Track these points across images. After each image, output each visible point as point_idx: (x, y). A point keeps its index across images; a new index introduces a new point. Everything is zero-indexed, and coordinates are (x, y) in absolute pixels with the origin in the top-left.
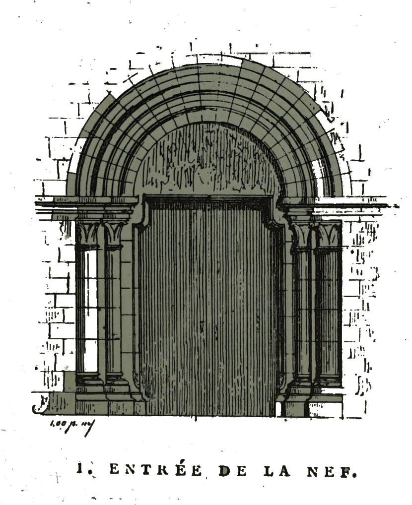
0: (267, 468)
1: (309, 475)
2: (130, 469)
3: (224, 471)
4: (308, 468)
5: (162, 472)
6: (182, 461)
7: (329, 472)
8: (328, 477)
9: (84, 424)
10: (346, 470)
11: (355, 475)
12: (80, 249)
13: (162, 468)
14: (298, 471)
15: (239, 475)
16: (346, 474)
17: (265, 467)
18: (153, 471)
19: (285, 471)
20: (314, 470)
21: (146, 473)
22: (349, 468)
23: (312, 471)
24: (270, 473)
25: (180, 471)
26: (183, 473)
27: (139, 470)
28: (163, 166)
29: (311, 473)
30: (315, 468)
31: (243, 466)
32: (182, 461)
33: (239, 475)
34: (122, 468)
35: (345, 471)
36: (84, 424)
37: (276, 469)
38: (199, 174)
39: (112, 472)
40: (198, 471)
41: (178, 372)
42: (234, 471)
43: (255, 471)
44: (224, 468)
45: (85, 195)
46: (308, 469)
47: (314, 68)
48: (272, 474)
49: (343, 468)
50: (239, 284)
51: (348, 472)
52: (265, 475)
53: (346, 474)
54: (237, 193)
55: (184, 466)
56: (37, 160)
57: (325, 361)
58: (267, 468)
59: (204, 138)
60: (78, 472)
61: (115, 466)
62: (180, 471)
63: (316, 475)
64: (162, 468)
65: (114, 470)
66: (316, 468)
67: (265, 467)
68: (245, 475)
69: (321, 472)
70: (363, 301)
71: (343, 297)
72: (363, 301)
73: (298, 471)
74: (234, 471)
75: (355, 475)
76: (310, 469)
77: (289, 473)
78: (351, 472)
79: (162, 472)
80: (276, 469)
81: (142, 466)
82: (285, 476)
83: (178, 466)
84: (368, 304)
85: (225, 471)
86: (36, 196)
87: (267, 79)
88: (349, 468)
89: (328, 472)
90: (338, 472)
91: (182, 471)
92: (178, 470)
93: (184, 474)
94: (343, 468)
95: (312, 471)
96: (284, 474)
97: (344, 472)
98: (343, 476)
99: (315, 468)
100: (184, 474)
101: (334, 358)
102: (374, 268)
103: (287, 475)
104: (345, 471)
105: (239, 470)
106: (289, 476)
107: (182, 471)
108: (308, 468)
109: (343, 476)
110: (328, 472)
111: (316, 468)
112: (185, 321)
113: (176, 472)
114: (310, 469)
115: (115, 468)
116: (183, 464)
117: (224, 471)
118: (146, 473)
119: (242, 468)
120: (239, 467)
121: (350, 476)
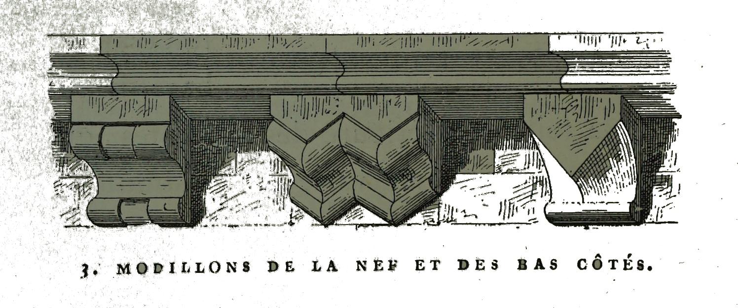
0: (315, 263)
1: (358, 270)
2: (232, 268)
3: (273, 266)
4: (227, 263)
6: (629, 255)
7: (289, 268)
9: (325, 216)
20: (363, 264)
23: (361, 265)
24: (201, 270)
26: (422, 268)
28: (577, 75)
30: (363, 261)
32: (629, 255)
34: (488, 265)
36: (325, 216)
37: (324, 264)
39: (417, 269)
42: (473, 265)
43: (259, 267)
44: (273, 264)
46: (357, 263)
48: (320, 269)
50: (300, 105)
55: (631, 261)
57: (333, 168)
58: (315, 263)
59: (664, 69)
60: (433, 269)
61: (482, 262)
63: (365, 269)
64: (523, 262)
66: (235, 263)
68: (423, 269)
69: (371, 266)
70: (672, 152)
72: (672, 152)
74: (473, 265)
76: (359, 262)
80: (324, 264)
82: (332, 270)
83: (625, 261)
84: (676, 154)
85: (274, 266)
91: (291, 268)
92: (287, 266)
95: (361, 265)
96: (539, 267)
99: (363, 261)
103: (335, 270)
105: (478, 264)
107: (291, 268)
108: (227, 263)
111: (365, 262)
113: (623, 267)
114: (359, 262)
115: (481, 264)
117: (273, 266)
118: (613, 268)
119: (480, 262)
120: (477, 261)
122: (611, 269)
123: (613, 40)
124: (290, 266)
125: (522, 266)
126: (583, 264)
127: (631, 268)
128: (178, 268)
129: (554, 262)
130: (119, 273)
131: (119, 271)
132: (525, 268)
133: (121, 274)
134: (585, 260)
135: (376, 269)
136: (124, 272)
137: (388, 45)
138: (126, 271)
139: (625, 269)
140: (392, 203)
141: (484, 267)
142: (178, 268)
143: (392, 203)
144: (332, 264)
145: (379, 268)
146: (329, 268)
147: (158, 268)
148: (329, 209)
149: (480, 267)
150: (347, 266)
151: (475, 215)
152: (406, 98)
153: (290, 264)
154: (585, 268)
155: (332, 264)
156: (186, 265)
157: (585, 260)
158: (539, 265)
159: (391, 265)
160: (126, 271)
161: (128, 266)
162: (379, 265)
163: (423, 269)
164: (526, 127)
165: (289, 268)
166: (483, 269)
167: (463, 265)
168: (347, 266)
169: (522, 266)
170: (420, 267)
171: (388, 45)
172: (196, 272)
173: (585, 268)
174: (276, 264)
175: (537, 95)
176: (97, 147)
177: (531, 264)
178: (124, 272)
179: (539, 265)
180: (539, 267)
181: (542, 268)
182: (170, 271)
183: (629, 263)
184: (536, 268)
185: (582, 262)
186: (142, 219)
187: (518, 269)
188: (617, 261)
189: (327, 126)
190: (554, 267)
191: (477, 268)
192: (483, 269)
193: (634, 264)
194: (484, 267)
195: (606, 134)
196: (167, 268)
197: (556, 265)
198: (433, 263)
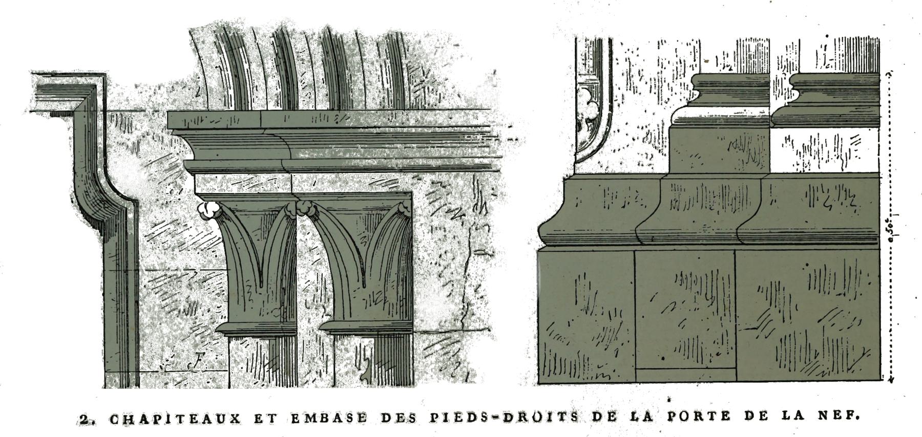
0: (785, 412)
1: (820, 418)
3: (749, 415)
7: (763, 416)
8: (295, 424)
11: (858, 418)
13: (128, 418)
15: (761, 419)
16: (850, 416)
17: (746, 412)
18: (186, 419)
19: (648, 417)
21: (562, 419)
22: (853, 411)
23: (823, 415)
27: (706, 417)
31: (401, 414)
33: (761, 419)
35: (850, 413)
37: (792, 414)
38: (677, 56)
40: (838, 415)
41: (318, 342)
46: (819, 414)
49: (848, 411)
51: (852, 415)
52: (783, 419)
53: (850, 416)
54: (300, 78)
56: (855, 151)
58: (785, 412)
63: (826, 418)
68: (766, 419)
69: (830, 415)
74: (757, 416)
75: (858, 418)
76: (821, 413)
77: (803, 417)
78: (855, 415)
79: (522, 419)
80: (792, 414)
81: (177, 416)
89: (837, 414)
90: (844, 414)
94: (848, 411)
95: (823, 415)
96: (206, 421)
97: (849, 415)
100: (461, 421)
102: (762, 40)
103: (801, 418)
104: (850, 413)
105: (192, 418)
106: (342, 422)
107: (297, 419)
109: (848, 418)
110: (837, 414)
112: (818, 277)
117: (749, 415)
118: (562, 419)
121: (853, 418)
122: (382, 422)
123: (785, 97)
124: (459, 417)
125: (324, 420)
126: (115, 420)
127: (461, 421)
128: (451, 417)
129: (349, 415)
130: (307, 422)
131: (820, 416)
132: (327, 420)
133: (308, 422)
134: (117, 416)
136: (311, 421)
138: (312, 420)
140: (735, 370)
142: (451, 417)
143: (735, 370)
144: (799, 413)
145: (401, 420)
146: (204, 421)
147: (485, 418)
148: (117, 343)
150: (811, 415)
153: (458, 415)
154: (117, 423)
155: (799, 413)
157: (117, 416)
158: (144, 419)
159: (649, 417)
160: (312, 420)
161: (314, 416)
162: (613, 416)
163: (766, 419)
165: (763, 416)
167: (725, 415)
168: (811, 415)
169: (324, 420)
170: (763, 418)
173: (117, 423)
175: (190, 127)
176: (595, 80)
178: (311, 421)
179: (144, 420)
180: (647, 419)
181: (340, 421)
182: (745, 417)
183: (764, 414)
184: (796, 419)
185: (115, 417)
186: (359, 349)
187: (668, 420)
188: (715, 413)
189: (63, 74)
192: (298, 422)
196: (442, 417)
198: (178, 417)
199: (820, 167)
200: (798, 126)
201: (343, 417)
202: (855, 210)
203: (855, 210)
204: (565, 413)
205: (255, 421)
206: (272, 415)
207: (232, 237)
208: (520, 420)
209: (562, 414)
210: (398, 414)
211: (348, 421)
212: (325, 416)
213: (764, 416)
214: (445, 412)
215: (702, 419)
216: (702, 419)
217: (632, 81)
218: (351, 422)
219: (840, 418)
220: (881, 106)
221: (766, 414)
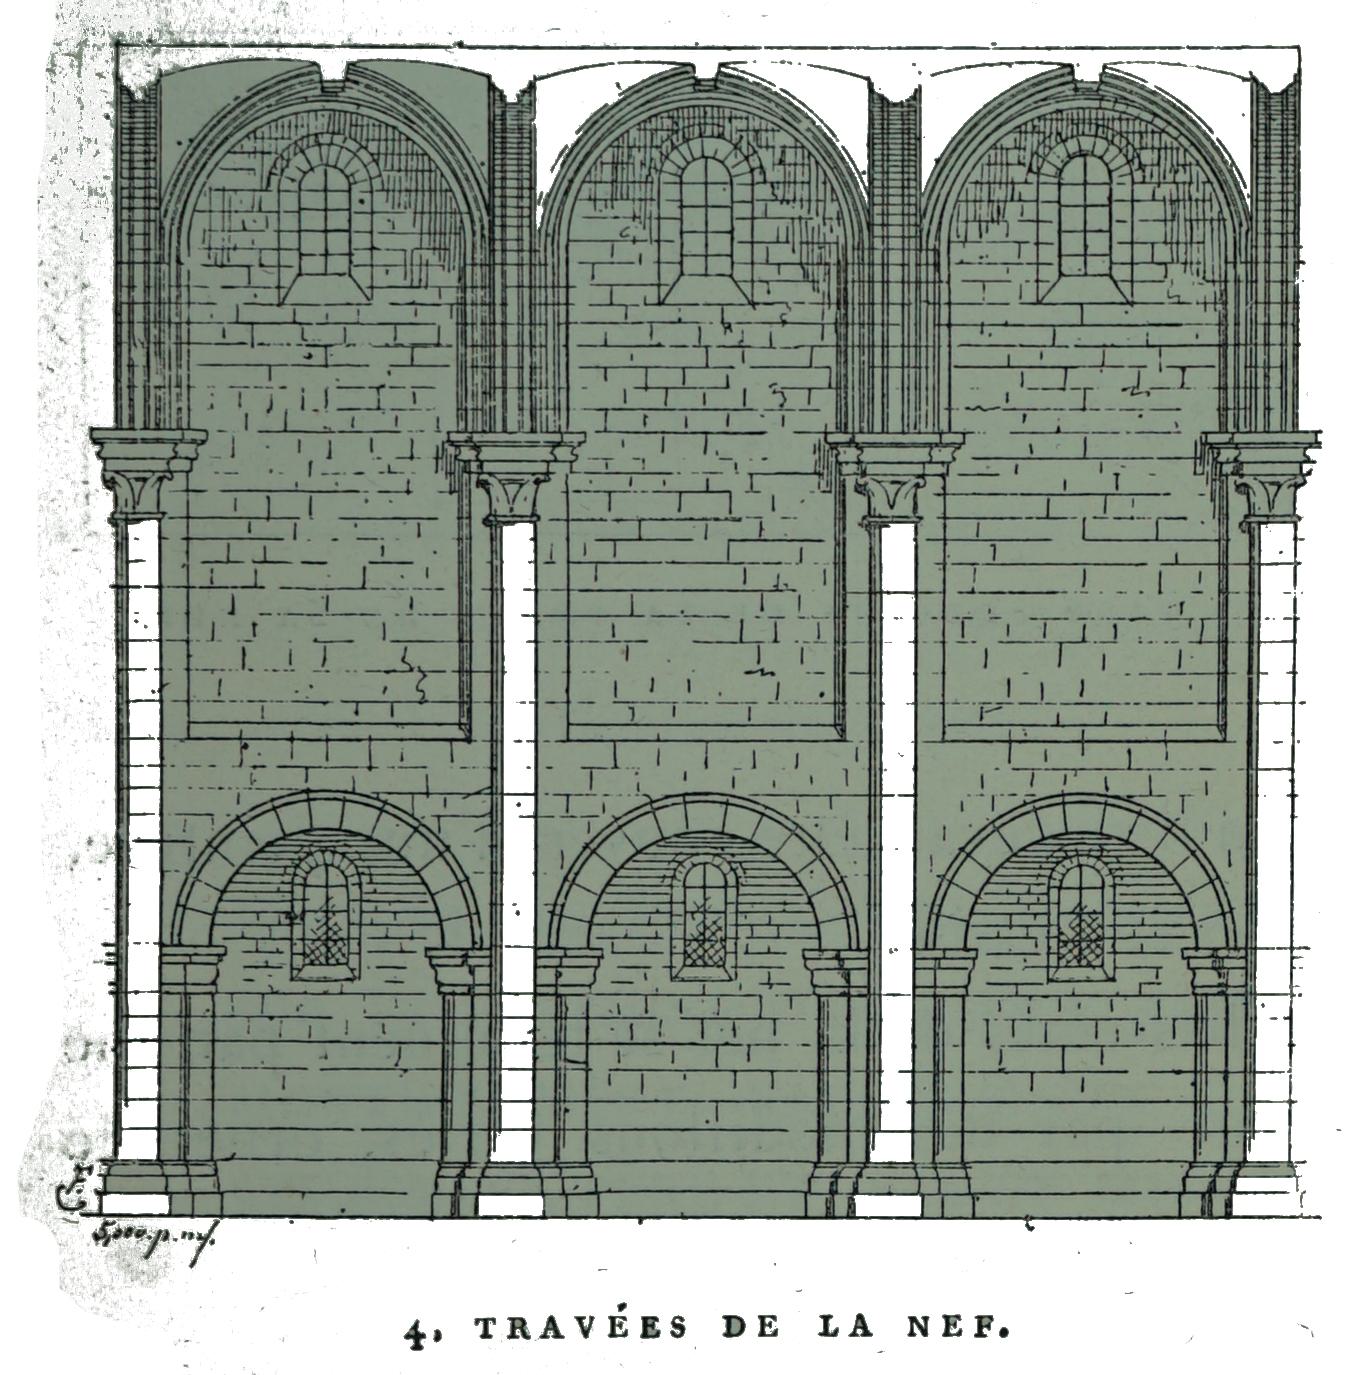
0: (826, 1318)
1: (912, 1334)
3: (734, 1326)
5: (518, 1332)
6: (622, 1307)
7: (617, 1328)
10: (650, 1322)
12: (121, 521)
14: (889, 1325)
17: (822, 1317)
18: (501, 1329)
19: (862, 1327)
22: (991, 1318)
23: (919, 1326)
24: (831, 1329)
25: (615, 1327)
26: (654, 1333)
29: (922, 1322)
34: (664, 1326)
35: (983, 1323)
37: (844, 1322)
43: (706, 1327)
44: (733, 1321)
45: (1243, 961)
47: (289, 345)
49: (980, 1318)
51: (989, 1327)
53: (985, 1331)
55: (624, 1318)
58: (826, 1318)
62: (615, 1327)
63: (925, 1333)
64: (518, 1323)
65: (649, 1329)
67: (822, 1317)
68: (775, 1333)
69: (936, 1326)
71: (132, 845)
73: (889, 1325)
74: (753, 1326)
75: (1004, 1333)
76: (913, 1320)
77: (562, 1333)
78: (996, 1327)
80: (844, 1322)
81: (477, 1321)
83: (612, 1319)
86: (437, 471)
87: (1048, 795)
88: (991, 1318)
89: (518, 1327)
90: (969, 1325)
93: (959, 1333)
94: (980, 1318)
97: (980, 1327)
98: (980, 1334)
101: (1089, 1177)
103: (867, 1333)
104: (983, 1323)
113: (609, 1331)
114: (913, 1320)
116: (622, 1314)
117: (734, 1326)
118: (486, 1335)
119: (767, 1320)
120: (762, 1318)
122: (976, 1336)
129: (677, 1321)
131: (926, 1323)
133: (517, 1337)
135: (947, 1334)
137: (326, 406)
139: (613, 1335)
141: (626, 1331)
145: (953, 1331)
149: (618, 1331)
151: (432, 1196)
152: (1129, 752)
156: (831, 1321)
158: (552, 1327)
159: (864, 1327)
164: (1014, 859)
166: (775, 1333)
171: (326, 406)
172: (821, 1334)
174: (741, 1320)
177: (536, 1326)
180: (859, 1331)
181: (558, 1335)
190: (678, 1332)
191: (762, 1334)
193: (635, 1326)
194: (626, 1331)
195: (1162, 861)
197: (682, 1329)
199: (380, 550)
200: (1256, 576)
201: (536, 1326)
202: (384, 692)
203: (384, 692)
204: (494, 1320)
205: (509, 1333)
206: (486, 1321)
207: (936, 895)
208: (512, 1336)
209: (950, 1321)
210: (762, 1318)
211: (673, 1334)
212: (518, 1323)
213: (770, 1325)
214: (826, 1313)
215: (526, 1336)
216: (526, 1336)
217: (184, 269)
218: (682, 1334)
219: (657, 1334)
220: (1300, 518)
221: (774, 1323)
